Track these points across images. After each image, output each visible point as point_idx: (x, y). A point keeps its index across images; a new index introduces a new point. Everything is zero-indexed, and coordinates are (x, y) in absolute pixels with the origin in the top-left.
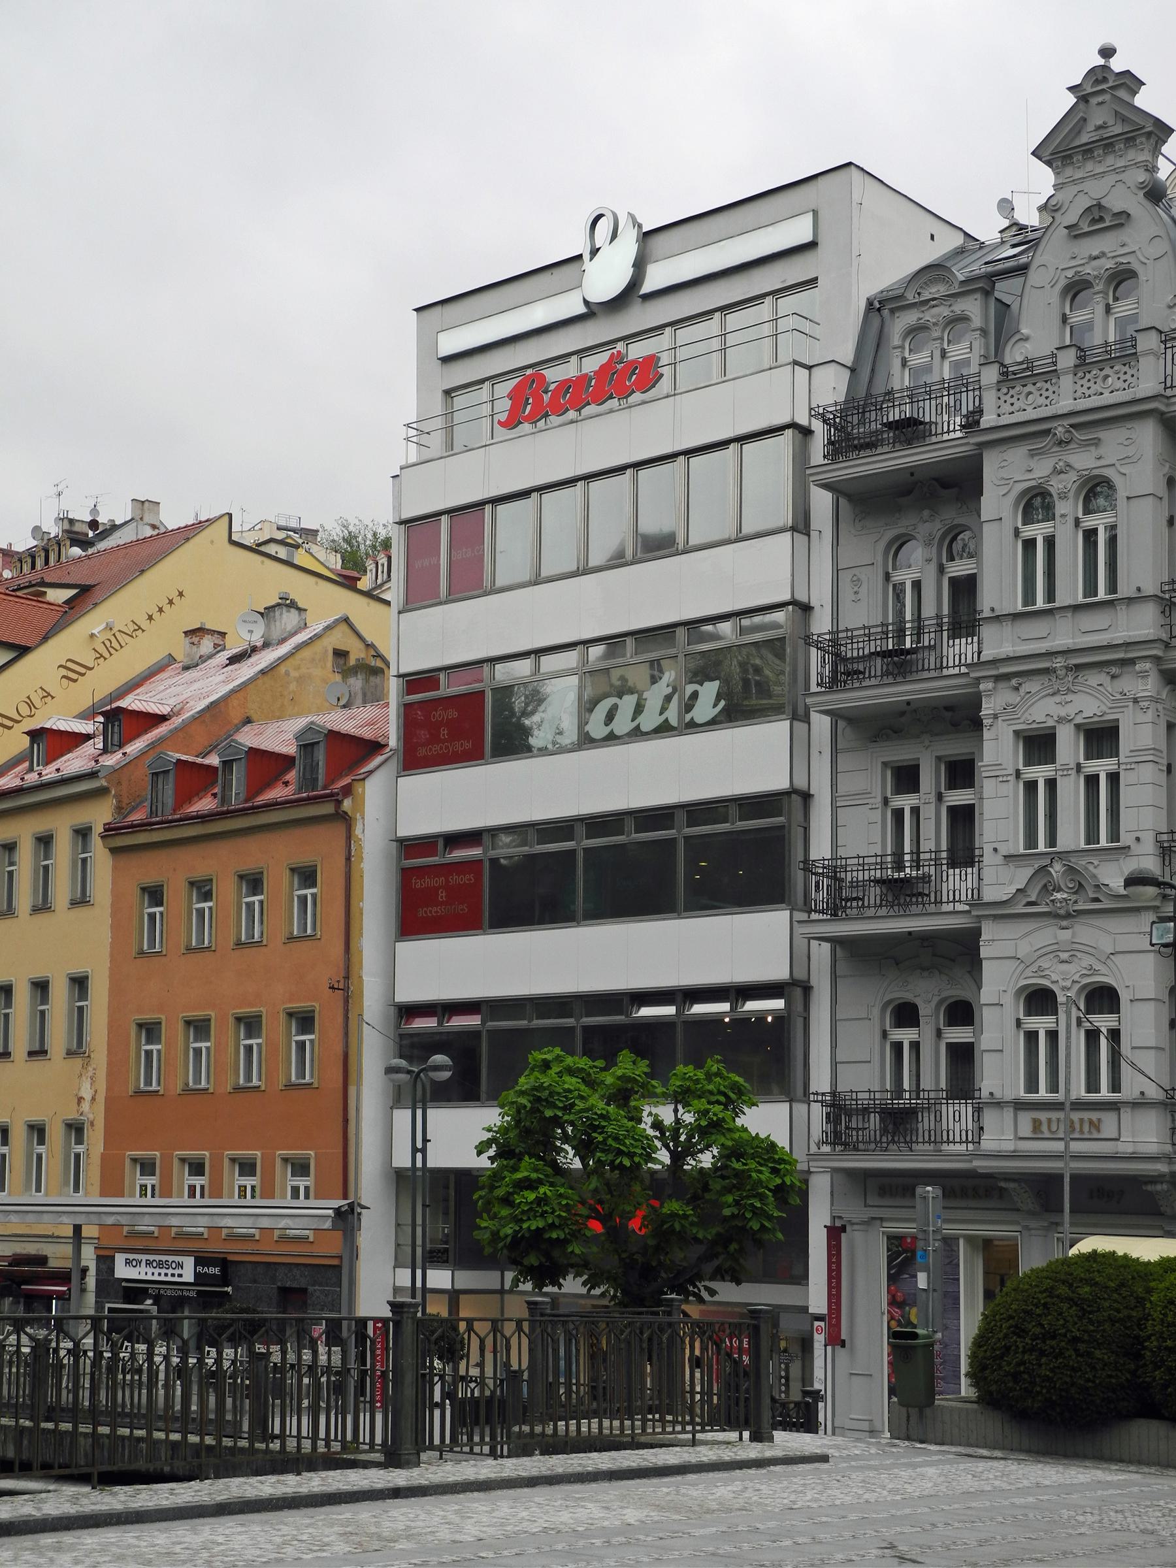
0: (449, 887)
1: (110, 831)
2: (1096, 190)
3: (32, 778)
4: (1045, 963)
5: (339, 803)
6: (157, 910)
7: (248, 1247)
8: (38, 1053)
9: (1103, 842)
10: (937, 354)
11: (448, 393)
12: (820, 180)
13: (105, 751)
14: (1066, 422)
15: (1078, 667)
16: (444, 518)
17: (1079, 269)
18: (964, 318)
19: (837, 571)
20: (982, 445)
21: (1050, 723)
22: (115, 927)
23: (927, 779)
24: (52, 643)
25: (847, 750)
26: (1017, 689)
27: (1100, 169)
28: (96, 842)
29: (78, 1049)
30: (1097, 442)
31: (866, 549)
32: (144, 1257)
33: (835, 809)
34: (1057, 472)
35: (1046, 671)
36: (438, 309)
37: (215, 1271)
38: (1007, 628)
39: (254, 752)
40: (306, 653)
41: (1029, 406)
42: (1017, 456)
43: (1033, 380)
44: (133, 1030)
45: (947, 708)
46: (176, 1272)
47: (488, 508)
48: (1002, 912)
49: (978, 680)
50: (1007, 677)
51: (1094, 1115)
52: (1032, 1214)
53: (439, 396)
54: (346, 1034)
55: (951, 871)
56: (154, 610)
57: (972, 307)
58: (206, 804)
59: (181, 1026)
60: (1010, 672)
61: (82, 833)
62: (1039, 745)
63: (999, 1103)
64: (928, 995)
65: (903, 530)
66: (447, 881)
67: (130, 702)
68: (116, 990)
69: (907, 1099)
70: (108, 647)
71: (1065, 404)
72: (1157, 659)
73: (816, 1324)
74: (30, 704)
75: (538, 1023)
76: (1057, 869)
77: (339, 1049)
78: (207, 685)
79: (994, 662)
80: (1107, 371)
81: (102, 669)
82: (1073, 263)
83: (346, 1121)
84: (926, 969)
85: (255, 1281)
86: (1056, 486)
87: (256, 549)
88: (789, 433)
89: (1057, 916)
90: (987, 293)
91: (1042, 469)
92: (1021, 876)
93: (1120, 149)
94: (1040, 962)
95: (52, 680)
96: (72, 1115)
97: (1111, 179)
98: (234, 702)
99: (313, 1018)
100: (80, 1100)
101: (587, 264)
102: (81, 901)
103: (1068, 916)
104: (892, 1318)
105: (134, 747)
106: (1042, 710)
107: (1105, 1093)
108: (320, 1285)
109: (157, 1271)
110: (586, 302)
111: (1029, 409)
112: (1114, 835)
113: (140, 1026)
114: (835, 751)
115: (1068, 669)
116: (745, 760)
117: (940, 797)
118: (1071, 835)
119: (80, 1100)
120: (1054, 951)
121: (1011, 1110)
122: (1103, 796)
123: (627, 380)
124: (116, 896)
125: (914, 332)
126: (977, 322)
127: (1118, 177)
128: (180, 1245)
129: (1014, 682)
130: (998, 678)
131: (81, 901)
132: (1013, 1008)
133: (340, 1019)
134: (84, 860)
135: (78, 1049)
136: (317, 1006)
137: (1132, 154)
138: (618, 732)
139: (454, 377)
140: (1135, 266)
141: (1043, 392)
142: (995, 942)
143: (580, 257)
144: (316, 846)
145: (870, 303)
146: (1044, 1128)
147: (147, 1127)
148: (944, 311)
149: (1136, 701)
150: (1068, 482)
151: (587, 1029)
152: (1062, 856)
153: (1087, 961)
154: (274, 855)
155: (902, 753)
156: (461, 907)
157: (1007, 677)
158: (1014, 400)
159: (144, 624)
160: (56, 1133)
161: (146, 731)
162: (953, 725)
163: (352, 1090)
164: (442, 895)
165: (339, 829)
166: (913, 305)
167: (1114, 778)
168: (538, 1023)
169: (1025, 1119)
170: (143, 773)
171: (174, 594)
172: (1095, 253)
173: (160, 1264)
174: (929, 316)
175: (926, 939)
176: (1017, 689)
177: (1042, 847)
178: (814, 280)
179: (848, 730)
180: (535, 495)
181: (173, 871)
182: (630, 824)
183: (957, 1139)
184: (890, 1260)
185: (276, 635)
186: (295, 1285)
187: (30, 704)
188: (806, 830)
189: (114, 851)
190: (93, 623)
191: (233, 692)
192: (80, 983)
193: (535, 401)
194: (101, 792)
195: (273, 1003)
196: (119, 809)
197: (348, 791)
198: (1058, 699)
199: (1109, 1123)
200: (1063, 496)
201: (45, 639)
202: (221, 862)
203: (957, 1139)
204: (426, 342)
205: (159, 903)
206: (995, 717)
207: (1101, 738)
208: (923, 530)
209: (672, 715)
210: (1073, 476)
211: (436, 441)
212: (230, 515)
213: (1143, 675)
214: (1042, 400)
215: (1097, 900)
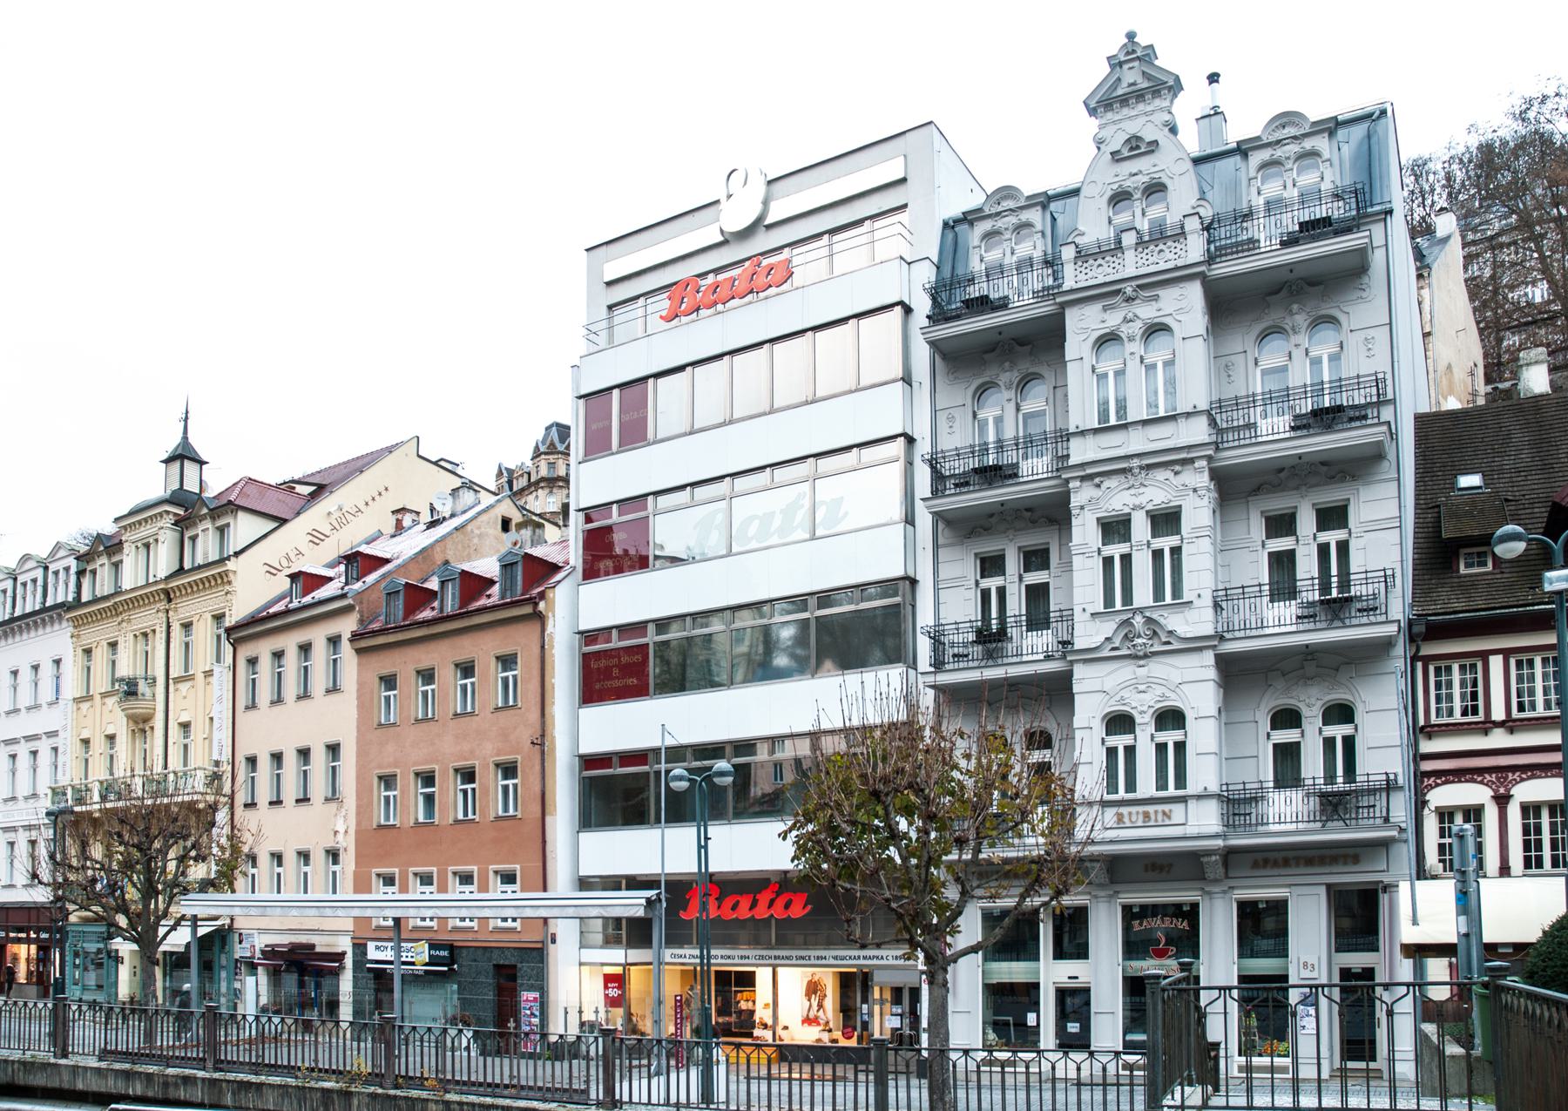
0: (615, 669)
1: (356, 637)
2: (1132, 128)
3: (295, 604)
4: (1126, 694)
5: (536, 604)
6: (391, 693)
7: (470, 936)
8: (304, 800)
9: (1168, 599)
10: (1008, 252)
11: (610, 307)
13: (347, 583)
14: (1134, 283)
15: (1149, 467)
18: (1028, 225)
19: (934, 412)
20: (1063, 306)
21: (1127, 510)
22: (361, 706)
23: (1013, 563)
24: (302, 517)
25: (945, 546)
26: (1098, 486)
27: (1133, 113)
28: (346, 646)
29: (333, 797)
30: (1156, 298)
31: (957, 395)
33: (937, 590)
34: (1126, 320)
35: (1123, 471)
37: (445, 953)
38: (1090, 439)
39: (464, 573)
40: (484, 517)
41: (1101, 273)
42: (1092, 312)
44: (376, 780)
45: (1323, 464)
47: (651, 381)
48: (1092, 657)
49: (1067, 481)
50: (1090, 477)
51: (1166, 807)
52: (1101, 886)
53: (605, 309)
54: (543, 778)
56: (375, 494)
57: (1034, 216)
58: (427, 614)
59: (412, 776)
60: (1094, 474)
61: (334, 641)
62: (1115, 528)
64: (1015, 728)
67: (365, 549)
68: (362, 753)
69: (1340, 784)
70: (341, 520)
71: (1131, 271)
72: (1209, 458)
74: (289, 559)
76: (1138, 621)
77: (537, 789)
78: (415, 541)
79: (1083, 465)
80: (1161, 246)
81: (335, 536)
83: (544, 842)
84: (1013, 708)
86: (1125, 331)
87: (436, 463)
88: (898, 309)
89: (1136, 657)
90: (1044, 207)
91: (1113, 320)
92: (1108, 628)
94: (1122, 693)
95: (303, 543)
96: (330, 844)
97: (1143, 119)
98: (438, 549)
100: (336, 833)
101: (724, 205)
102: (334, 689)
103: (1146, 656)
105: (371, 578)
106: (1117, 498)
107: (1172, 791)
110: (722, 231)
112: (1177, 592)
113: (380, 778)
114: (936, 546)
115: (1141, 468)
117: (1021, 578)
118: (1143, 594)
119: (336, 833)
120: (1134, 685)
122: (1169, 567)
123: (763, 278)
124: (361, 685)
125: (988, 236)
126: (1039, 227)
128: (415, 936)
129: (1097, 480)
130: (1083, 479)
131: (334, 689)
132: (1099, 729)
133: (538, 768)
134: (335, 661)
135: (333, 797)
137: (1157, 102)
139: (620, 297)
140: (1165, 180)
142: (1085, 679)
143: (717, 202)
144: (519, 640)
145: (946, 225)
146: (1126, 819)
147: (383, 850)
148: (1012, 220)
149: (1195, 490)
150: (1136, 328)
152: (1141, 610)
153: (1159, 690)
154: (484, 648)
155: (989, 546)
157: (1090, 477)
159: (363, 507)
160: (318, 857)
161: (375, 569)
163: (548, 819)
164: (615, 671)
165: (535, 627)
166: (990, 216)
167: (1176, 551)
169: (1110, 813)
170: (379, 596)
171: (382, 489)
173: (803, 958)
174: (1001, 223)
175: (1013, 684)
176: (1098, 486)
177: (1118, 605)
178: (905, 206)
180: (689, 369)
181: (405, 663)
182: (651, 628)
185: (459, 508)
187: (289, 559)
188: (914, 606)
189: (359, 651)
190: (328, 503)
191: (437, 541)
192: (334, 749)
193: (686, 299)
194: (348, 609)
195: (484, 757)
196: (361, 621)
197: (542, 596)
198: (1132, 491)
199: (1177, 811)
200: (1131, 339)
201: (298, 514)
202: (443, 656)
204: (594, 271)
205: (393, 688)
206: (1082, 508)
207: (1165, 521)
208: (1004, 378)
210: (1139, 324)
211: (602, 340)
213: (1199, 470)
214: (1172, 256)
215: (1169, 643)
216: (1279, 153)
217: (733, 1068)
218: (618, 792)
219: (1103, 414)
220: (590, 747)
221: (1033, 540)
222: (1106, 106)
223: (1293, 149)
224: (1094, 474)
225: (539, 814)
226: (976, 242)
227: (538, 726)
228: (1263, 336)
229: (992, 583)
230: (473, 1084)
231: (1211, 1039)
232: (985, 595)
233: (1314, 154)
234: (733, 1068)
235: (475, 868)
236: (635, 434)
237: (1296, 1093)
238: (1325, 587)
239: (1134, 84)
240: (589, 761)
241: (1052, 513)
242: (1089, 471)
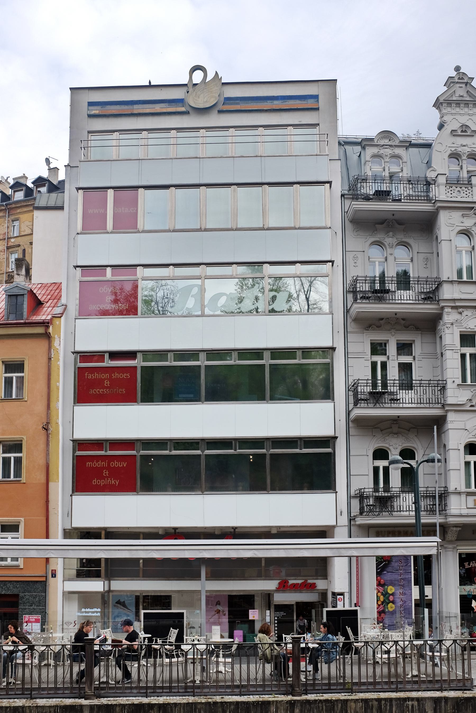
0: (103, 380)
2: (464, 120)
5: (48, 327)
12: (319, 82)
16: (110, 192)
17: (457, 148)
36: (87, 91)
43: (457, 185)
45: (403, 319)
48: (459, 409)
49: (443, 308)
55: (401, 391)
60: (458, 306)
63: (460, 493)
65: (378, 239)
66: (111, 376)
73: (338, 597)
75: (174, 452)
77: (41, 461)
82: (453, 145)
83: (47, 501)
93: (471, 107)
97: (468, 117)
99: (21, 445)
104: (379, 592)
108: (29, 592)
111: (459, 197)
121: (465, 495)
127: (470, 117)
129: (461, 310)
130: (453, 307)
136: (25, 438)
138: (276, 309)
141: (465, 192)
151: (271, 455)
155: (379, 337)
156: (121, 390)
158: (452, 192)
162: (405, 327)
163: (51, 484)
164: (107, 383)
165: (43, 344)
166: (377, 145)
168: (174, 452)
172: (464, 144)
175: (396, 420)
176: (461, 313)
179: (353, 323)
182: (202, 356)
183: (405, 510)
184: (377, 565)
186: (9, 593)
203: (405, 510)
209: (262, 305)
214: (464, 195)
216: (382, 151)
218: (103, 468)
219: (460, 273)
220: (82, 433)
221: (405, 337)
222: (448, 103)
223: (389, 151)
224: (458, 306)
225: (43, 480)
226: (368, 158)
227: (44, 415)
228: (373, 243)
229: (379, 359)
230: (364, 684)
232: (374, 365)
233: (398, 157)
236: (127, 223)
237: (171, 663)
238: (374, 385)
239: (462, 96)
240: (80, 444)
241: (429, 325)
242: (458, 304)
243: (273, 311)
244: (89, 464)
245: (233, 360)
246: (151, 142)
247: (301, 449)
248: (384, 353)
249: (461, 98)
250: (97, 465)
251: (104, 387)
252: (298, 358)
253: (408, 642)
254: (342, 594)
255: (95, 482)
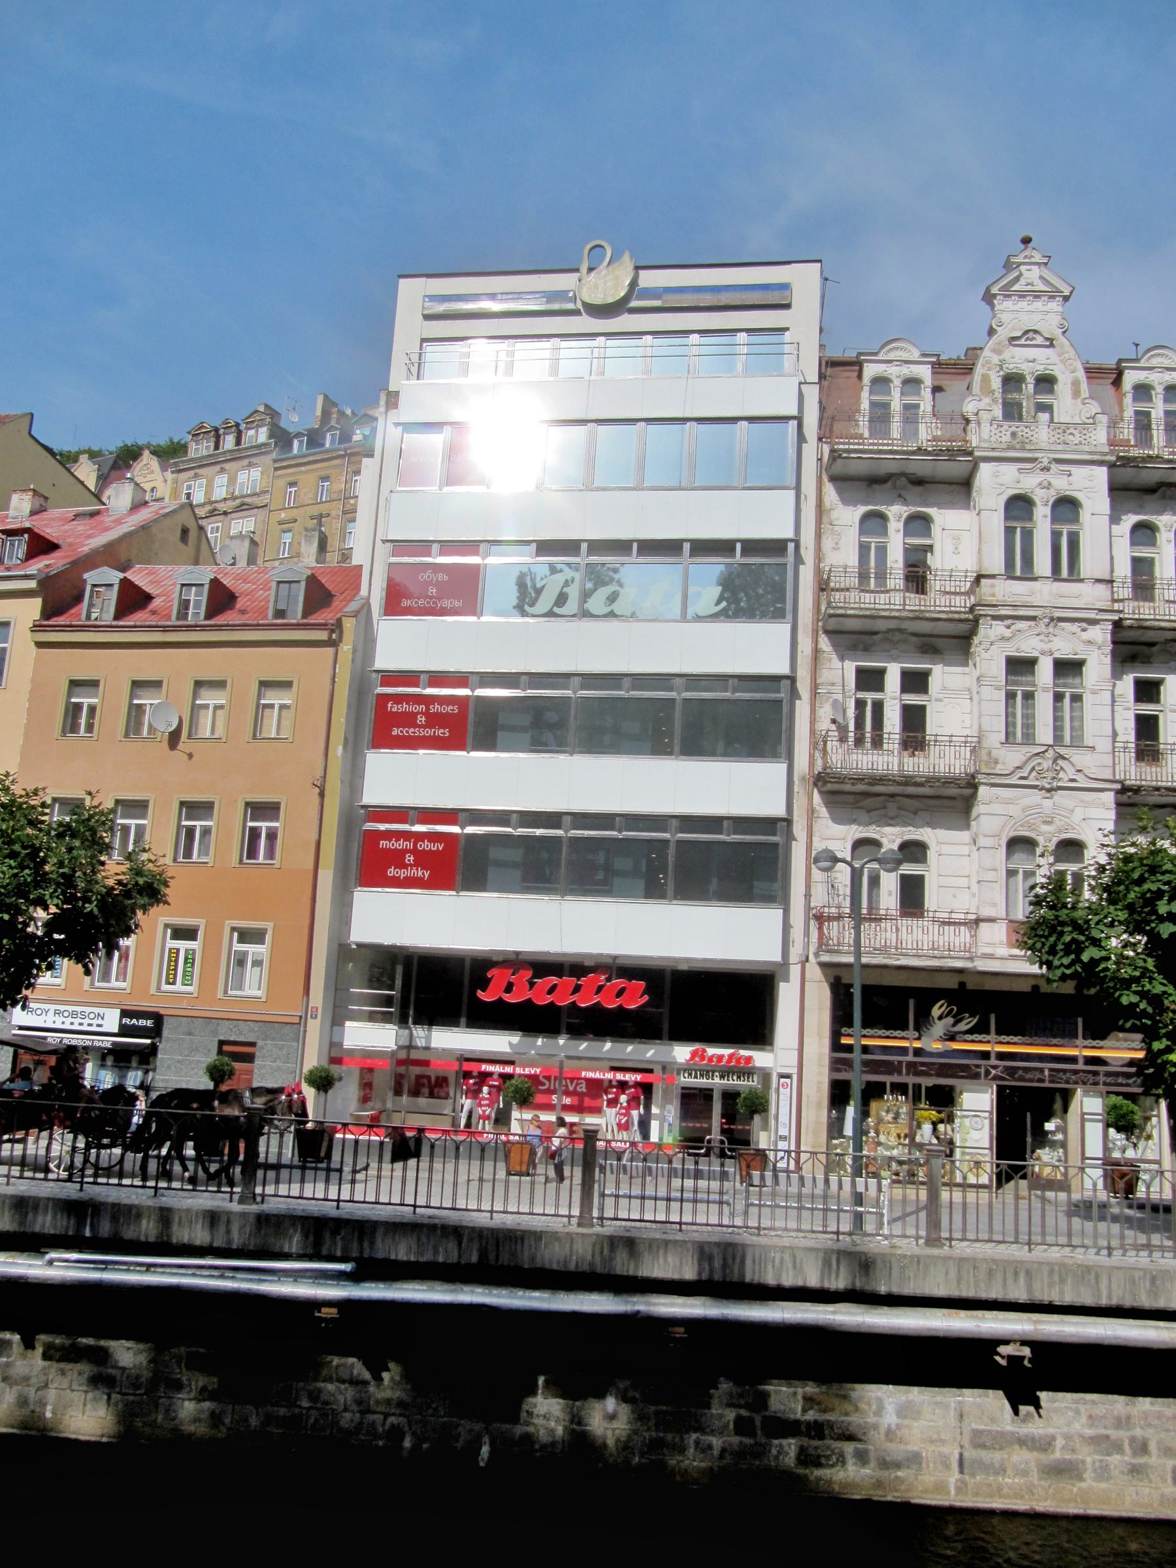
21: (1035, 654)
32: (53, 1007)
35: (1034, 618)
46: (95, 1022)
66: (428, 709)
85: (190, 1034)
99: (278, 808)
106: (1028, 644)
108: (273, 1039)
109: (70, 1020)
116: (756, 648)
129: (1009, 622)
151: (679, 842)
156: (442, 731)
164: (421, 720)
172: (1031, 358)
173: (74, 1014)
176: (1008, 627)
182: (626, 682)
207: (1068, 668)
212: (32, 415)
217: (487, 1187)
225: (310, 865)
229: (869, 697)
231: (956, 986)
234: (487, 1187)
235: (204, 921)
243: (612, 615)
244: (383, 844)
245: (730, 689)
246: (609, 352)
247: (620, 831)
248: (880, 687)
249: (1029, 288)
250: (396, 845)
251: (415, 726)
252: (522, 685)
253: (782, 1154)
254: (788, 1076)
255: (391, 872)
